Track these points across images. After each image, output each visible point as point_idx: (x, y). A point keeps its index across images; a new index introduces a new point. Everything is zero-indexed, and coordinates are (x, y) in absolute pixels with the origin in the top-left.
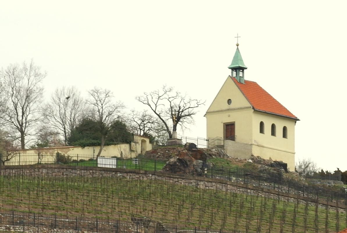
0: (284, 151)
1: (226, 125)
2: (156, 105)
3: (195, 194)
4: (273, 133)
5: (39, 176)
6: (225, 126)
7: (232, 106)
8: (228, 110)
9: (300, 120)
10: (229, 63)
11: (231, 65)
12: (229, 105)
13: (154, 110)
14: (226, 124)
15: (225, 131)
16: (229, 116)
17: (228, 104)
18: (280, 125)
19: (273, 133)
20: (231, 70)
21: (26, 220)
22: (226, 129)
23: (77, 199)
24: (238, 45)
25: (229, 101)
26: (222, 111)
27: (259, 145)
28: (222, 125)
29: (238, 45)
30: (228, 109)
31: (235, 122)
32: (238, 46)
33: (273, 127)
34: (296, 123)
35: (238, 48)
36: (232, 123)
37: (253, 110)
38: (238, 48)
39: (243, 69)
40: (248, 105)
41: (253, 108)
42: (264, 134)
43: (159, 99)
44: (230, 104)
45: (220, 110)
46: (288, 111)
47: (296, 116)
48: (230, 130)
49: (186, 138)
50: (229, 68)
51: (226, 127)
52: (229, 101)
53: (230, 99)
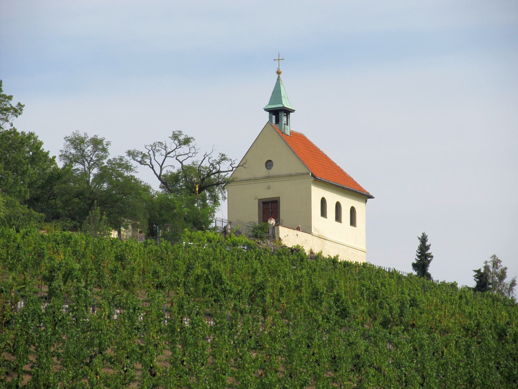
0: (353, 247)
1: (262, 202)
2: (161, 167)
3: (38, 264)
4: (338, 218)
5: (231, 328)
6: (261, 204)
7: (274, 171)
8: (268, 177)
9: (374, 198)
10: (265, 101)
11: (270, 104)
12: (269, 171)
13: (158, 174)
14: (264, 201)
15: (262, 213)
16: (269, 188)
17: (265, 169)
18: (347, 203)
19: (338, 218)
20: (268, 113)
21: (89, 368)
22: (264, 209)
23: (31, 301)
24: (279, 73)
25: (269, 164)
26: (255, 179)
27: (320, 236)
28: (256, 202)
29: (279, 73)
30: (268, 176)
31: (279, 198)
32: (280, 75)
33: (338, 206)
34: (366, 201)
35: (279, 77)
36: (275, 199)
37: (312, 179)
38: (279, 77)
39: (287, 112)
40: (303, 169)
41: (313, 175)
42: (327, 218)
43: (166, 157)
44: (270, 169)
45: (253, 177)
46: (355, 182)
47: (368, 191)
48: (271, 210)
49: (222, 222)
50: (266, 110)
51: (263, 207)
52: (269, 164)
53: (270, 161)
